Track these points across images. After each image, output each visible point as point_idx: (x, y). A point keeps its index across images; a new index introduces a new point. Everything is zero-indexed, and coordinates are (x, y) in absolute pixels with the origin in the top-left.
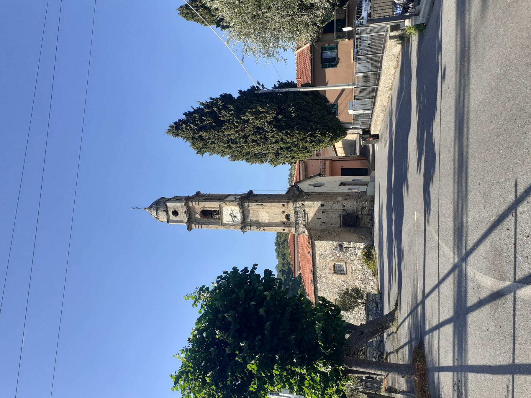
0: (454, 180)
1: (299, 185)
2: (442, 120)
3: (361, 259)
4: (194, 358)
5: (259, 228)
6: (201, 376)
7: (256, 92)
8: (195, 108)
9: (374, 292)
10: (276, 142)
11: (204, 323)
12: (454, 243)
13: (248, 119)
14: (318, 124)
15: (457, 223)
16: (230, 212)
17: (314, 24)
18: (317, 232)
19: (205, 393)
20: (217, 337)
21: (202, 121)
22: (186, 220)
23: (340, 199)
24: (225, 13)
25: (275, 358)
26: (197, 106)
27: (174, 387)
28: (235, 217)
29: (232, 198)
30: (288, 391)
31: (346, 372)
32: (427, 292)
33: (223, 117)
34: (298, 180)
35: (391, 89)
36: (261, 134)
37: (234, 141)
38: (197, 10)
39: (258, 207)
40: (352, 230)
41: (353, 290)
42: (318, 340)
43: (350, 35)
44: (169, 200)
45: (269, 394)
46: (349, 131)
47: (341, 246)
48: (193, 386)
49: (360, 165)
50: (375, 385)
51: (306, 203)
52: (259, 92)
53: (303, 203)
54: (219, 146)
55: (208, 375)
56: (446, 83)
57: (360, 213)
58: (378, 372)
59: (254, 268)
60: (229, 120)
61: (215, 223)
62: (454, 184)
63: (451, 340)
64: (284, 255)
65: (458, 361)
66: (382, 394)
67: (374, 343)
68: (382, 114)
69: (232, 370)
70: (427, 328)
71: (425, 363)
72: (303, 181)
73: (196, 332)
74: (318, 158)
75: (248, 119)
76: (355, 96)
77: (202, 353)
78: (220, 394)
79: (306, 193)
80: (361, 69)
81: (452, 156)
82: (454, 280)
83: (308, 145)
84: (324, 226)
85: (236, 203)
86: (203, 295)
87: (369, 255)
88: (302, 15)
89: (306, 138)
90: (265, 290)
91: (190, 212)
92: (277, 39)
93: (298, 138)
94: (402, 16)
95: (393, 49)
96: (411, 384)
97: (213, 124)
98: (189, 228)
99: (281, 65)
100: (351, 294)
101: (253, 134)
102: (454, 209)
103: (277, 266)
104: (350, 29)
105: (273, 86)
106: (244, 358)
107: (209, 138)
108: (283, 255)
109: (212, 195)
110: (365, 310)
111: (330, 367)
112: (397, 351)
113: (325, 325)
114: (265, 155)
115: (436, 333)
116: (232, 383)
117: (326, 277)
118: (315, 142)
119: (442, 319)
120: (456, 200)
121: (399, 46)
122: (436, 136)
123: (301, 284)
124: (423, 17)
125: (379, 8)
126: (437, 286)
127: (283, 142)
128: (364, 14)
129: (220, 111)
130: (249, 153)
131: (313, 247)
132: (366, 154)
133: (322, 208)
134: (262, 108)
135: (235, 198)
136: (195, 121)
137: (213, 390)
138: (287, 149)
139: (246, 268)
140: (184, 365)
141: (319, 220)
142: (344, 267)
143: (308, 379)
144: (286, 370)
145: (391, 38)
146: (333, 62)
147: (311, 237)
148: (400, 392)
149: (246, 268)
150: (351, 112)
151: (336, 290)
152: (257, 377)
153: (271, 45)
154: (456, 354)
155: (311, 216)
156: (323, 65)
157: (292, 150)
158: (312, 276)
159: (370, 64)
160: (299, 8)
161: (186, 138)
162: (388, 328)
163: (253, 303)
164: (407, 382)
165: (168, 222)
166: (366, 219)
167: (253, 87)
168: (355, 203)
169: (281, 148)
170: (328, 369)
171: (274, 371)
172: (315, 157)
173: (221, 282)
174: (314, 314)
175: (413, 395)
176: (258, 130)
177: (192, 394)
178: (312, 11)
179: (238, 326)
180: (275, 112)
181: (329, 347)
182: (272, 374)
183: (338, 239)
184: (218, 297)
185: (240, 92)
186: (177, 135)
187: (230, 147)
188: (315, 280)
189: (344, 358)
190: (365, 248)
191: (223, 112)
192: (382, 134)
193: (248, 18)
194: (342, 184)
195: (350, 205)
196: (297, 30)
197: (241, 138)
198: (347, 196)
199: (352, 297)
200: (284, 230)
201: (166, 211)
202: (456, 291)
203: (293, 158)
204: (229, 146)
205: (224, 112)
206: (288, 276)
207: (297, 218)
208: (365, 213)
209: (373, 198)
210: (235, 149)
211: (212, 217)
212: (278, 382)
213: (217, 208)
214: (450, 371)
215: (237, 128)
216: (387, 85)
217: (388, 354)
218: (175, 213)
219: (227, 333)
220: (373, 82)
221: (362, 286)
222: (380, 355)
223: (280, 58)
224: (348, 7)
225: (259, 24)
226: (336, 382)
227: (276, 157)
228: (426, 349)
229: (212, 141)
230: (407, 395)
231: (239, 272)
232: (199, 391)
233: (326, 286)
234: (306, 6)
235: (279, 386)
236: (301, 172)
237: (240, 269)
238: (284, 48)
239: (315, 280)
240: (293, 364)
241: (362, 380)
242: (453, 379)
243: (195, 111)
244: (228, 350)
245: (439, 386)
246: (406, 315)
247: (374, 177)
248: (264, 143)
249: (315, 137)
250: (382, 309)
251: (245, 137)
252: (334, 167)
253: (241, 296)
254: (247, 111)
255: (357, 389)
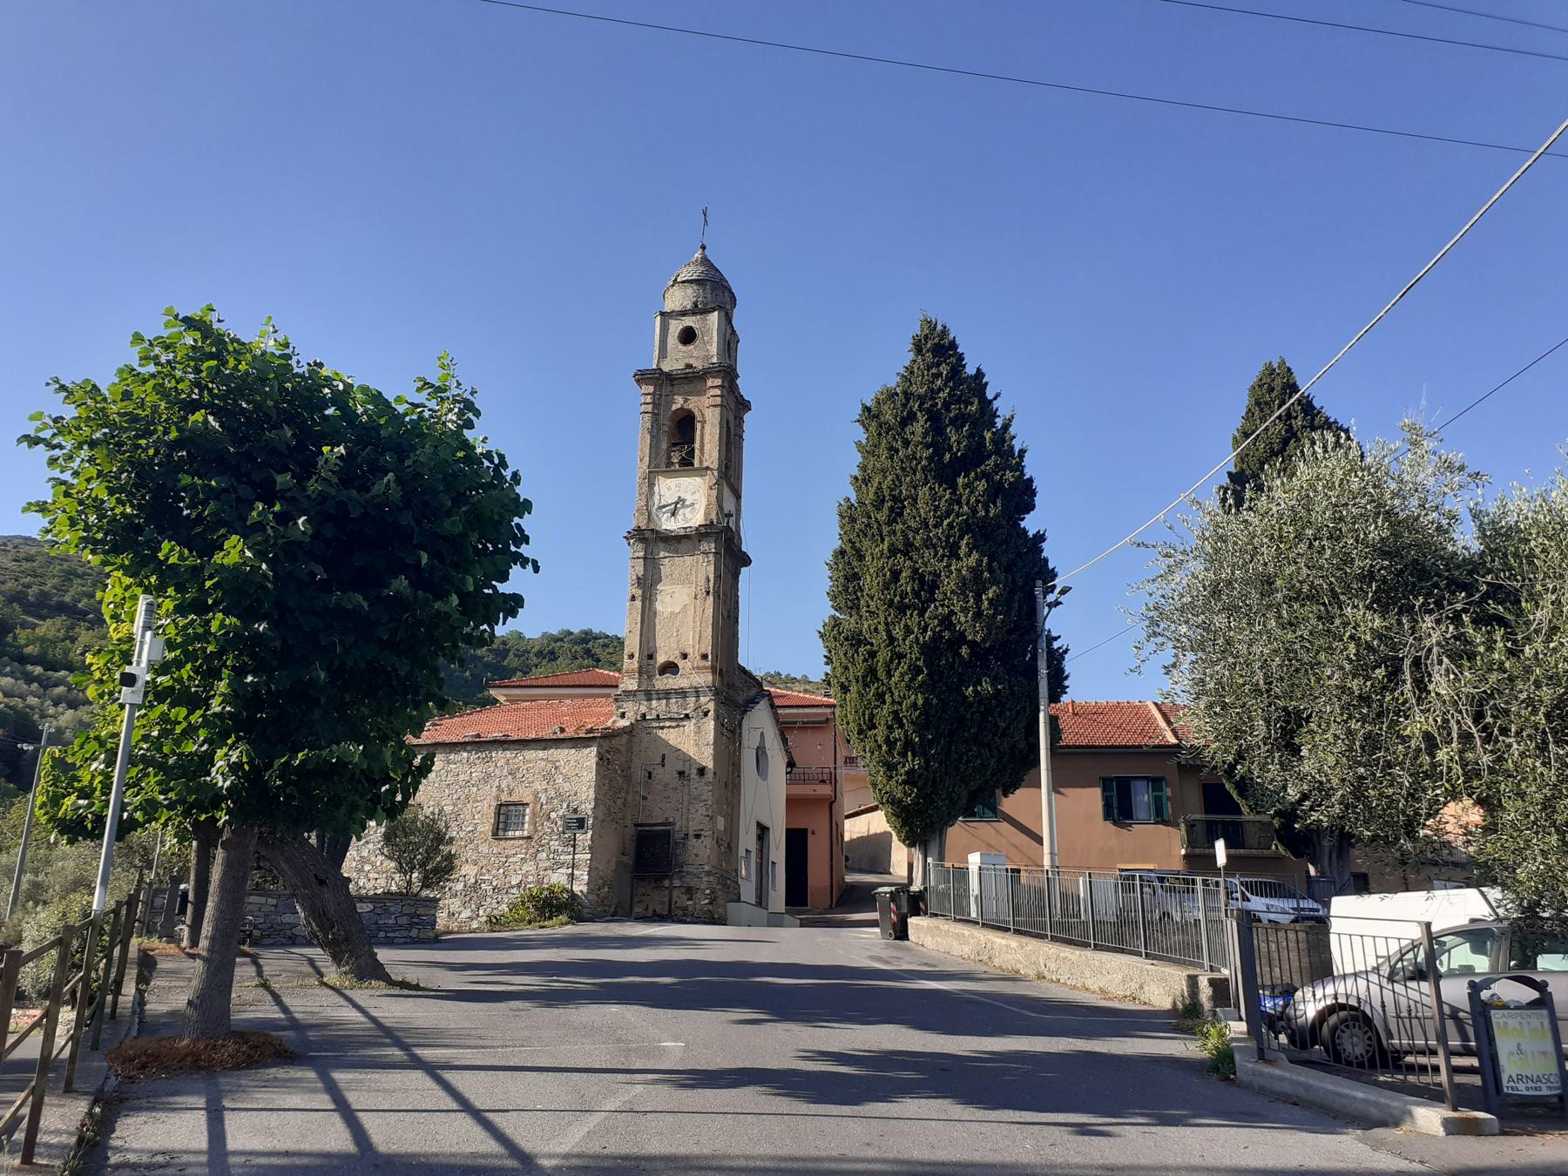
0: (785, 1159)
1: (763, 705)
2: (959, 1124)
3: (540, 882)
4: (264, 380)
5: (640, 582)
6: (207, 397)
7: (1039, 583)
8: (996, 404)
9: (442, 920)
10: (892, 639)
11: (366, 412)
12: (596, 1157)
13: (959, 559)
14: (940, 763)
15: (658, 1164)
16: (688, 499)
17: (1240, 757)
18: (622, 755)
19: (155, 408)
20: (326, 449)
21: (958, 422)
22: (666, 368)
23: (721, 823)
24: (1280, 494)
25: (260, 621)
26: (1003, 408)
27: (176, 317)
28: (673, 514)
29: (729, 505)
30: (157, 657)
31: (207, 835)
32: (449, 1076)
33: (966, 486)
34: (777, 702)
35: (1041, 977)
36: (916, 594)
37: (896, 514)
38: (1279, 417)
39: (702, 581)
40: (625, 859)
41: (450, 858)
42: (311, 749)
43: (1199, 861)
44: (727, 319)
45: (150, 598)
46: (918, 855)
47: (581, 823)
48: (178, 374)
49: (819, 883)
50: (160, 920)
51: (710, 725)
52: (1038, 591)
53: (711, 714)
54: (884, 471)
55: (211, 418)
56: (1066, 1137)
57: (677, 883)
58: (207, 929)
59: (524, 562)
60: (959, 503)
61: (657, 454)
62: (772, 1158)
63: (306, 1146)
64: (553, 656)
65: (243, 1166)
66: (135, 942)
67: (288, 918)
68: (966, 950)
69: (225, 490)
70: (338, 1076)
71: (231, 1069)
72: (776, 715)
73: (341, 387)
74: (840, 762)
75: (959, 559)
76: (1019, 871)
77: (276, 402)
78: (151, 452)
79: (740, 725)
80: (1096, 891)
81: (854, 1153)
82: (485, 1156)
83: (880, 733)
84: (639, 775)
85: (713, 516)
86: (451, 410)
87: (550, 905)
88: (1267, 721)
89: (902, 726)
90: (462, 596)
91: (692, 379)
92: (1198, 646)
93: (900, 704)
94: (1256, 1017)
95: (1157, 985)
96: (164, 1024)
97: (948, 456)
98: (643, 377)
99: (1119, 657)
100: (437, 851)
101: (915, 571)
102: (698, 1157)
103: (520, 636)
104: (1221, 857)
105: (1054, 634)
106: (260, 526)
107: (906, 443)
108: (552, 653)
109: (741, 448)
110: (388, 894)
111: (228, 783)
112: (265, 986)
113: (354, 774)
114: (854, 607)
115: (325, 1101)
116: (184, 489)
117: (487, 778)
118: (890, 752)
119: (366, 1120)
120: (726, 1163)
121: (1167, 1005)
122: (911, 1106)
123: (466, 704)
124: (1254, 1073)
125: (1273, 946)
126: (466, 1106)
127: (891, 661)
128: (1257, 903)
129: (985, 475)
130: (861, 558)
131: (577, 742)
132: (853, 899)
133: (694, 771)
134: (991, 601)
135: (729, 515)
136: (959, 401)
137: (166, 432)
138: (872, 671)
139: (526, 540)
140: (242, 348)
141: (659, 760)
142: (518, 834)
143: (193, 719)
144: (222, 652)
145: (1193, 981)
146: (1119, 810)
147: (610, 735)
148: (140, 993)
149: (526, 540)
150: (974, 860)
151: (448, 809)
152: (202, 566)
153: (1183, 629)
154: (262, 1161)
155: (671, 736)
156: (1111, 780)
157: (866, 685)
158: (490, 737)
159: (1113, 919)
160: (1288, 713)
161: (908, 376)
162: (337, 958)
163: (425, 558)
164: (173, 1014)
165: (662, 314)
166: (657, 901)
167: (1053, 575)
168: (707, 868)
169: (873, 654)
170: (220, 778)
171: (220, 616)
172: (842, 753)
173: (486, 463)
174: (384, 739)
175: (134, 1033)
176: (927, 586)
177: (152, 368)
178: (1279, 750)
179: (356, 513)
180: (978, 639)
181: (287, 783)
182: (209, 609)
183: (601, 817)
184: (444, 453)
185: (1040, 537)
186: (918, 348)
187: (879, 503)
188: (478, 744)
189: (252, 826)
190: (573, 895)
191: (981, 486)
192: (908, 949)
193: (1266, 564)
194: (763, 831)
195: (701, 853)
196: (1224, 706)
197: (905, 536)
198: (727, 844)
199: (429, 854)
200: (631, 656)
201: (696, 310)
202: (452, 1161)
203: (845, 689)
204: (883, 501)
205: (981, 488)
206: (487, 666)
207: (667, 694)
208: (675, 898)
209: (721, 921)
210: (874, 519)
211: (674, 445)
212: (185, 627)
213: (701, 461)
214: (210, 1141)
215: (935, 526)
216: (1053, 966)
217: (255, 960)
218: (688, 336)
219: (335, 480)
220: (1062, 926)
221: (460, 886)
222: (250, 936)
223: (1144, 654)
224: (1278, 858)
225: (1244, 596)
226: (181, 801)
227: (846, 639)
228: (273, 1070)
229: (897, 451)
230: (134, 1012)
231: (516, 520)
232: (160, 390)
233: (462, 777)
234: (1293, 731)
235: (172, 631)
236: (801, 711)
237: (526, 522)
238: (1174, 666)
239: (478, 744)
240: (240, 672)
241: (177, 881)
242: (186, 1152)
243: (986, 404)
244: (284, 479)
245: (163, 1110)
246: (375, 1013)
247: (781, 926)
248: (891, 604)
249: (903, 754)
250: (390, 943)
251: (908, 549)
252: (813, 808)
253: (447, 524)
254: (982, 554)
255: (149, 865)
